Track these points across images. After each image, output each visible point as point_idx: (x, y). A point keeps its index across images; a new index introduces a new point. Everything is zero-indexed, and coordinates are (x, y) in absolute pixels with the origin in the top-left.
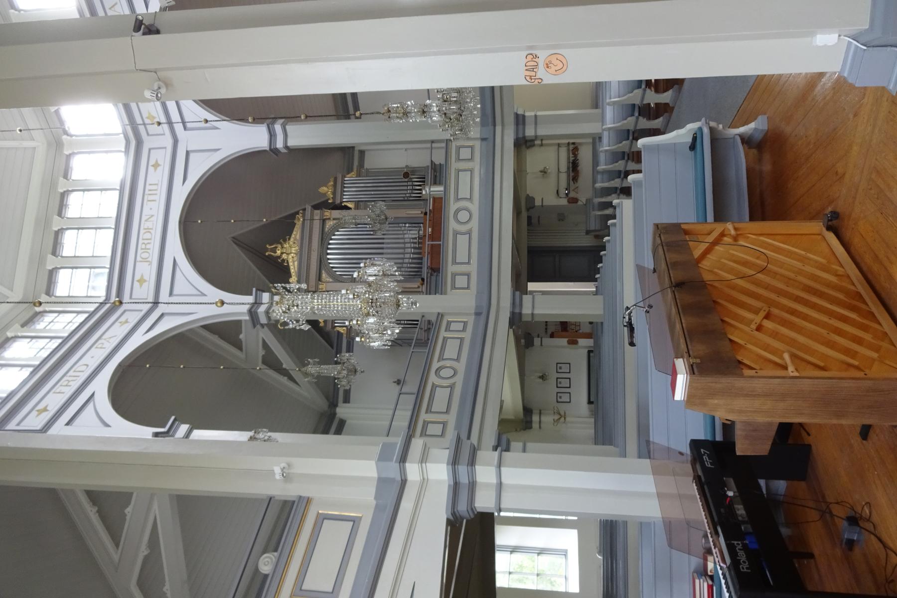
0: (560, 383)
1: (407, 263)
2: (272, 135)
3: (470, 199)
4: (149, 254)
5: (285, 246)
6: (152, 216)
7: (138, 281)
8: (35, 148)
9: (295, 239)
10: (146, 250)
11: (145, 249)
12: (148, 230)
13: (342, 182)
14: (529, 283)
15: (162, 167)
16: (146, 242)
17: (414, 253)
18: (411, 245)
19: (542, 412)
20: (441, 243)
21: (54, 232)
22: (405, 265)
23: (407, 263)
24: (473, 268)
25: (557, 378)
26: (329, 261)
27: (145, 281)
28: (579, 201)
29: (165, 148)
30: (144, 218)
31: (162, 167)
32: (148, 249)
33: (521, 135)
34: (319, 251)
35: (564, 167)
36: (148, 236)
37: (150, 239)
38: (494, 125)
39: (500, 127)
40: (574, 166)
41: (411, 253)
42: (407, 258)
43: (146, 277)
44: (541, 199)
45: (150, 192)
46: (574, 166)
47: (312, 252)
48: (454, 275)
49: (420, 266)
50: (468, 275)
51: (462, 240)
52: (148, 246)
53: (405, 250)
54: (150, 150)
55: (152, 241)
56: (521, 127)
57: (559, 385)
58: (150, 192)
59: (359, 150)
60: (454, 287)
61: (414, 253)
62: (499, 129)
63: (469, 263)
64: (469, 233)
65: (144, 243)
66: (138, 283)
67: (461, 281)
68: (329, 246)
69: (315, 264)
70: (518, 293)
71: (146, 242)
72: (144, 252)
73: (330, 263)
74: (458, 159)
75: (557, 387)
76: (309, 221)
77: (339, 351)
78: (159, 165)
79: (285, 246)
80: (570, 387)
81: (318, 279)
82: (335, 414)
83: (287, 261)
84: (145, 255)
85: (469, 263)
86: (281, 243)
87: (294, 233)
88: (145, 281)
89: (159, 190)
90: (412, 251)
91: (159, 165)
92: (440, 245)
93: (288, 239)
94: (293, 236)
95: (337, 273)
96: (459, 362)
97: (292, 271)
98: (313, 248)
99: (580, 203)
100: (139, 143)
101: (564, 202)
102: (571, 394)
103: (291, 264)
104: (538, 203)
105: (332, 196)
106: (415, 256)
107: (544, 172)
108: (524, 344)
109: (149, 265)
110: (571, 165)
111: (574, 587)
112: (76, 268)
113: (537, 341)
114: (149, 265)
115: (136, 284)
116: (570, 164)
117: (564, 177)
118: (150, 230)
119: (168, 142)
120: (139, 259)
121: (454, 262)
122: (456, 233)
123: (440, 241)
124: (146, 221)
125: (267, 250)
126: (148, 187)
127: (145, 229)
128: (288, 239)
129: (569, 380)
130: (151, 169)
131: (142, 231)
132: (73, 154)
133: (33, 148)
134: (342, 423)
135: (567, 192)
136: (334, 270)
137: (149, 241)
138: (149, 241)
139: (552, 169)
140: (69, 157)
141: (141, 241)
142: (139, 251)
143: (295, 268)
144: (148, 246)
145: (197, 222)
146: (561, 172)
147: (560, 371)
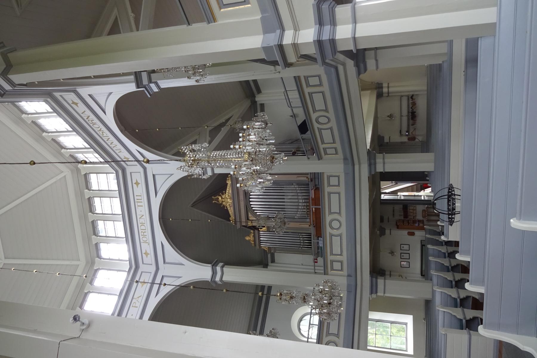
0: (403, 256)
1: (300, 212)
2: (214, 273)
3: (339, 213)
4: (147, 238)
5: (223, 197)
6: (143, 215)
7: (135, 183)
8: (65, 176)
9: (229, 193)
10: (144, 236)
11: (144, 235)
12: (143, 224)
13: (258, 233)
14: (381, 182)
15: (141, 184)
16: (143, 231)
17: (304, 202)
18: (302, 197)
19: (391, 273)
20: (320, 207)
21: (83, 176)
22: (299, 210)
23: (300, 212)
24: (344, 258)
25: (401, 253)
26: (251, 203)
27: (148, 254)
28: (416, 139)
29: (151, 273)
30: (138, 217)
31: (141, 184)
32: (145, 235)
33: (373, 173)
34: (245, 201)
35: (405, 112)
36: (143, 227)
37: (145, 230)
38: (353, 165)
39: (358, 166)
40: (413, 116)
41: (303, 203)
42: (299, 212)
43: (148, 252)
44: (388, 138)
45: (138, 201)
46: (413, 116)
47: (241, 202)
48: (329, 194)
49: (311, 244)
50: (341, 262)
51: (336, 240)
52: (145, 234)
53: (298, 204)
54: (142, 272)
55: (146, 231)
56: (373, 166)
57: (402, 258)
58: (138, 201)
59: (260, 104)
60: (332, 269)
61: (304, 202)
62: (357, 167)
63: (339, 185)
64: (340, 236)
65: (142, 232)
66: (136, 185)
67: (337, 266)
68: (251, 197)
69: (243, 209)
70: (374, 279)
71: (143, 231)
72: (143, 237)
73: (252, 207)
74: (329, 185)
75: (401, 258)
76: (239, 222)
77: (256, 112)
78: (139, 184)
79: (223, 197)
80: (409, 259)
81: (246, 218)
82: (256, 102)
83: (226, 207)
84: (145, 239)
85: (339, 185)
86: (220, 196)
87: (228, 189)
88: (148, 254)
89: (143, 199)
90: (303, 205)
91: (139, 184)
92: (320, 208)
93: (224, 193)
94: (227, 191)
95: (258, 214)
96: (338, 154)
97: (230, 213)
98: (240, 199)
99: (417, 140)
100: (137, 267)
101: (405, 139)
102: (410, 245)
103: (229, 209)
104: (386, 140)
105: (253, 243)
106: (306, 201)
107: (391, 116)
108: (379, 234)
109: (148, 245)
110: (410, 114)
111: (411, 351)
112: (99, 173)
113: (387, 232)
114: (148, 245)
115: (144, 255)
116: (410, 113)
117: (405, 119)
118: (144, 224)
119: (153, 269)
120: (141, 241)
121: (332, 254)
122: (331, 235)
123: (320, 206)
124: (140, 218)
125: (213, 200)
126: (136, 198)
127: (140, 223)
128: (224, 193)
129: (408, 258)
130: (135, 186)
131: (139, 225)
132: (99, 269)
133: (64, 176)
134: (262, 105)
135: (407, 134)
136: (255, 211)
137: (145, 231)
138: (145, 231)
139: (397, 114)
140: (96, 271)
141: (140, 231)
142: (141, 237)
143: (232, 211)
144: (145, 234)
145: (170, 219)
146: (403, 116)
147: (403, 249)
